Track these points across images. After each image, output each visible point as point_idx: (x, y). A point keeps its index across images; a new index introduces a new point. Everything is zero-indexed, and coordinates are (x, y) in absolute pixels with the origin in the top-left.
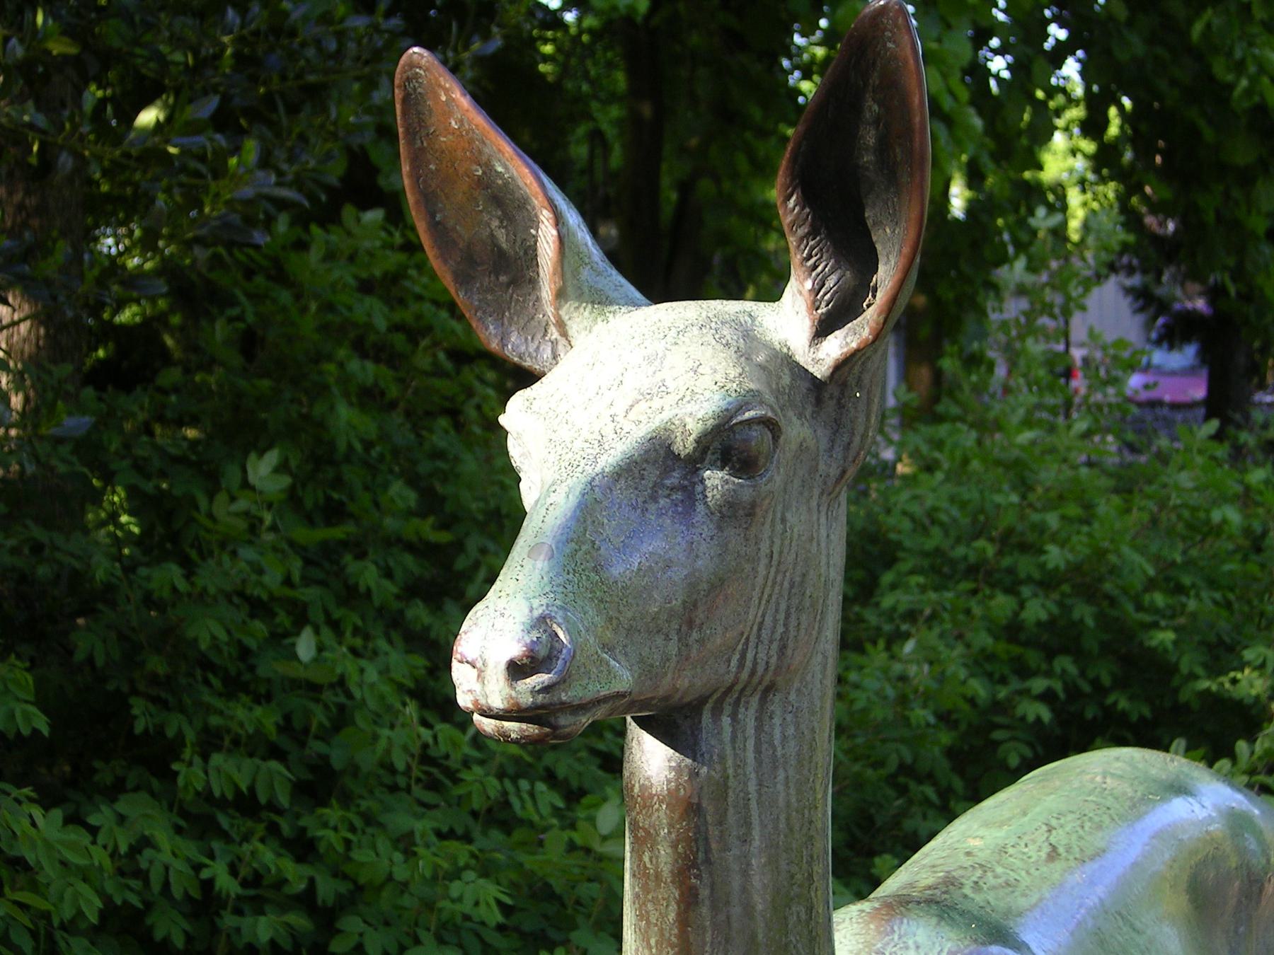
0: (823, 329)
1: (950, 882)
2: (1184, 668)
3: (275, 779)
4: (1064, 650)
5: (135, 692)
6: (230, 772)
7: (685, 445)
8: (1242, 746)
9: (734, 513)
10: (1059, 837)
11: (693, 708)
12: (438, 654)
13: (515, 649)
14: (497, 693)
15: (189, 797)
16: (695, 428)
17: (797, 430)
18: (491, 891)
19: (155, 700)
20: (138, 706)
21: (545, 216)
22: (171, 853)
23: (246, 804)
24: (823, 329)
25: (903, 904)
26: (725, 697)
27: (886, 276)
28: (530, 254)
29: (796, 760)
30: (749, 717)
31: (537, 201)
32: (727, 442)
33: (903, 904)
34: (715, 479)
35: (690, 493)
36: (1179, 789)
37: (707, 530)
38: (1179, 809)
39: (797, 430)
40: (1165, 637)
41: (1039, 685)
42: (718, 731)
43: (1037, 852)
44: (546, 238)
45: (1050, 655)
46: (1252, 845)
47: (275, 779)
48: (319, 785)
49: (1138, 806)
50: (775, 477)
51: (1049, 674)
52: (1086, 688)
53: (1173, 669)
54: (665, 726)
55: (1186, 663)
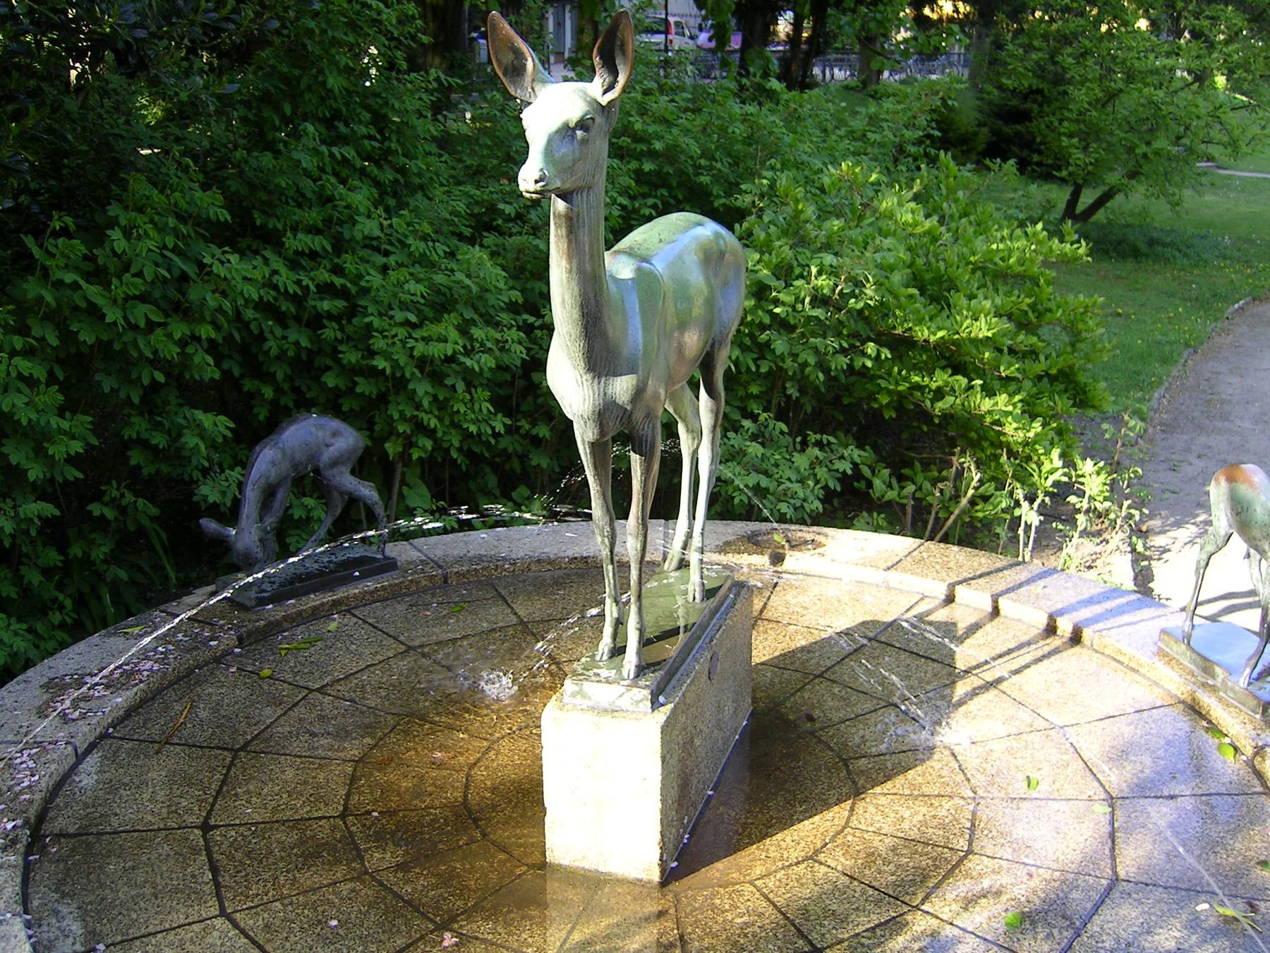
0: (605, 92)
1: (631, 248)
2: (715, 192)
3: (318, 243)
4: (663, 186)
5: (254, 207)
6: (304, 241)
7: (572, 125)
8: (737, 226)
9: (584, 142)
10: (662, 237)
11: (571, 193)
12: (514, 179)
13: (537, 177)
14: (532, 187)
15: (291, 252)
16: (575, 120)
17: (599, 120)
18: (420, 288)
19: (264, 212)
20: (256, 214)
21: (530, 59)
22: (286, 278)
23: (313, 255)
24: (605, 92)
25: (618, 252)
26: (579, 190)
27: (622, 79)
28: (524, 67)
29: (597, 204)
30: (585, 195)
31: (527, 55)
32: (582, 124)
33: (618, 252)
34: (579, 133)
35: (573, 136)
36: (700, 224)
37: (577, 146)
38: (699, 231)
39: (599, 120)
40: (705, 179)
41: (650, 201)
42: (577, 199)
43: (656, 240)
44: (530, 65)
45: (657, 187)
46: (722, 242)
47: (318, 243)
48: (340, 245)
49: (687, 229)
50: (593, 132)
51: (656, 197)
52: (672, 202)
53: (711, 194)
54: (564, 196)
55: (716, 190)
